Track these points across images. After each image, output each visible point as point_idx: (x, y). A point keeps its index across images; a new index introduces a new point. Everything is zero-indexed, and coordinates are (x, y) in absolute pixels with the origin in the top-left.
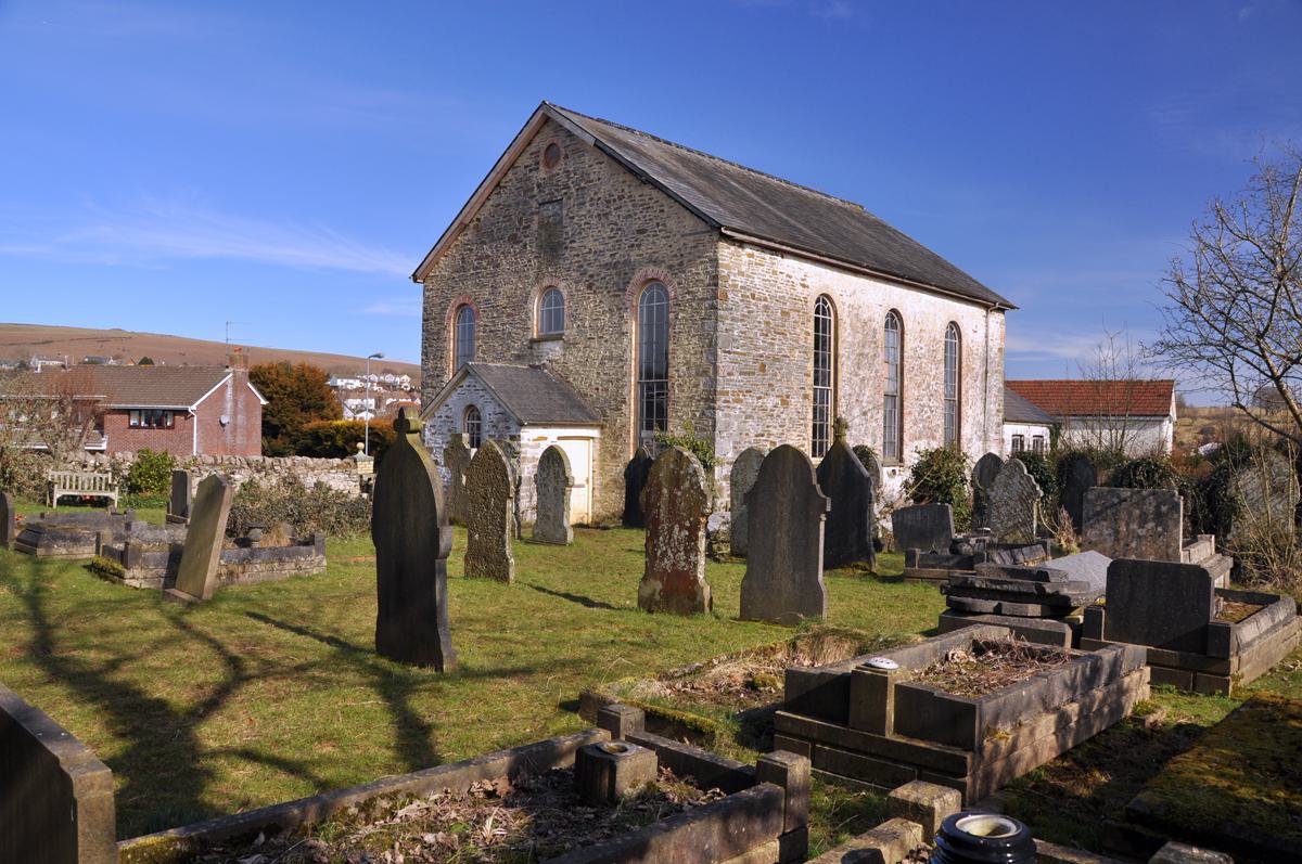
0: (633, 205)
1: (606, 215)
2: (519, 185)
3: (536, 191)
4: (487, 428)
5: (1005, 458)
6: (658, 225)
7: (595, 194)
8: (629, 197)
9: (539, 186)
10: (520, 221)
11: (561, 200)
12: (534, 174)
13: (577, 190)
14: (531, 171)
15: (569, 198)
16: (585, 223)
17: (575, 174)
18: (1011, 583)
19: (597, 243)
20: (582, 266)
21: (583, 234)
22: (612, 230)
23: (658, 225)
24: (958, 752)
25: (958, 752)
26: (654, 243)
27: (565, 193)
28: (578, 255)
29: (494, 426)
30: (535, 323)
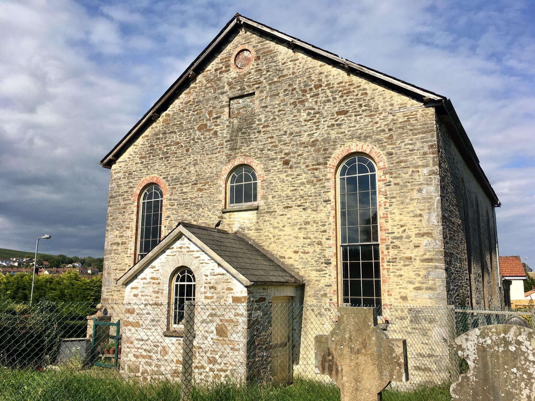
0: (332, 92)
1: (302, 102)
2: (209, 85)
3: (227, 88)
4: (203, 290)
5: (378, 317)
6: (360, 106)
7: (290, 85)
8: (326, 85)
9: (229, 84)
10: (210, 113)
11: (253, 94)
12: (225, 75)
13: (270, 84)
14: (221, 73)
15: (262, 92)
16: (279, 111)
17: (268, 71)
18: (174, 185)
19: (292, 126)
20: (276, 146)
21: (278, 120)
22: (309, 114)
23: (360, 106)
24: (365, 91)
25: (365, 91)
26: (356, 121)
27: (258, 88)
28: (272, 137)
29: (211, 288)
30: (439, 264)
